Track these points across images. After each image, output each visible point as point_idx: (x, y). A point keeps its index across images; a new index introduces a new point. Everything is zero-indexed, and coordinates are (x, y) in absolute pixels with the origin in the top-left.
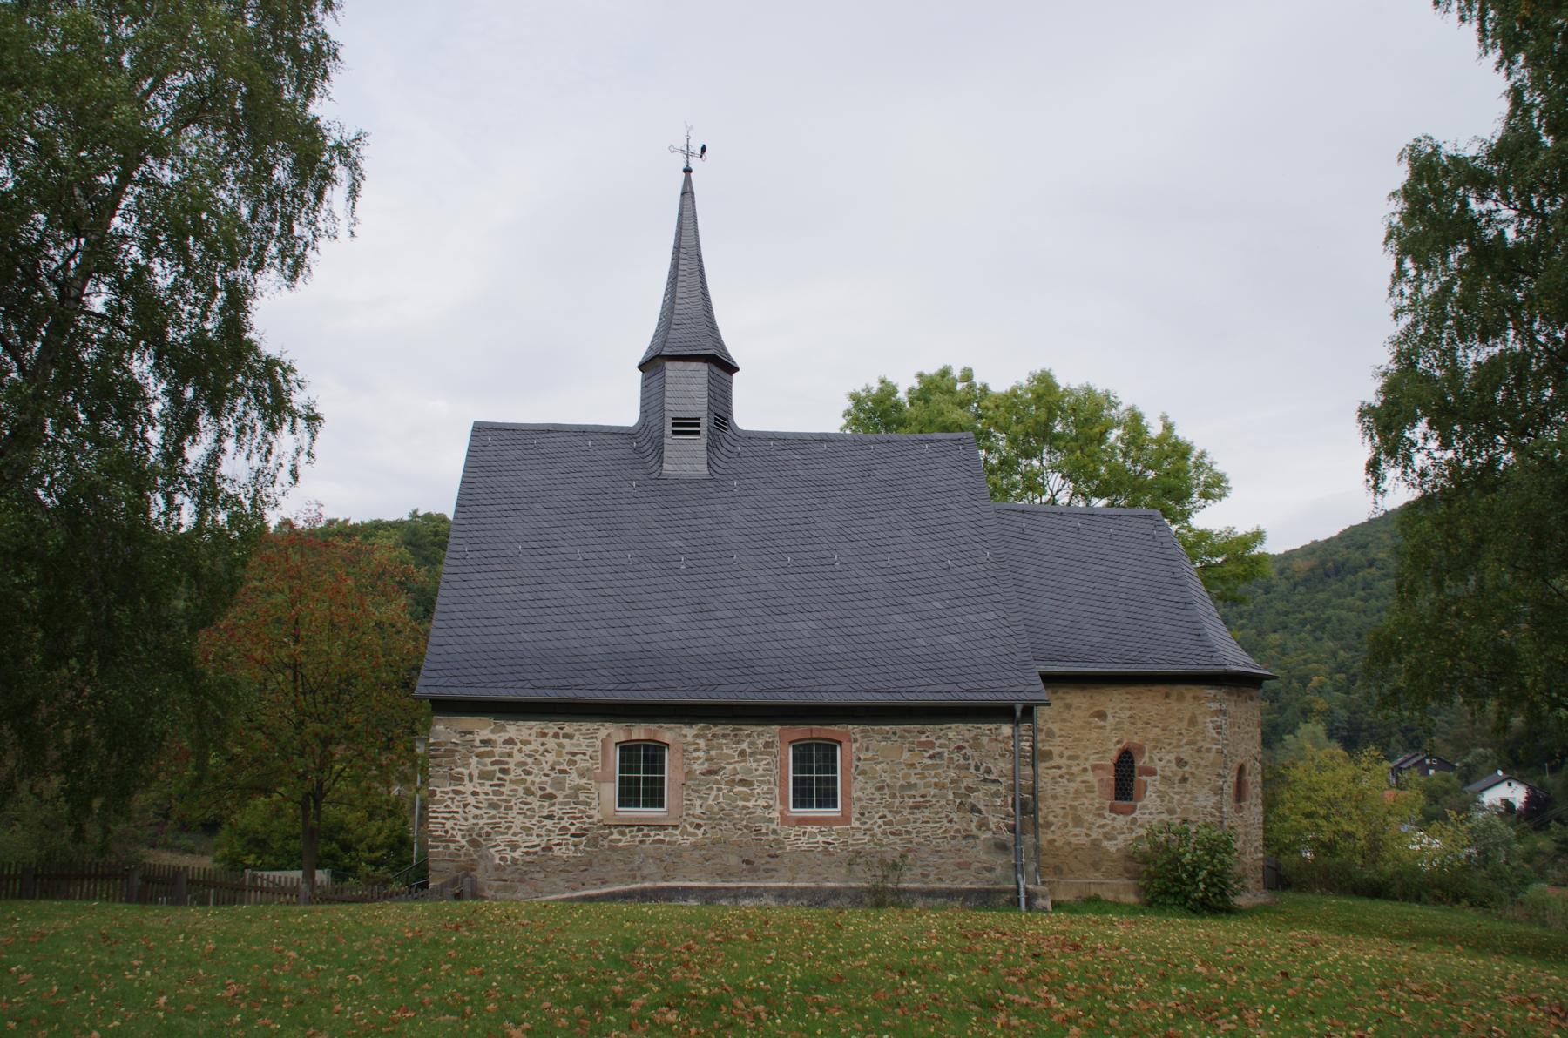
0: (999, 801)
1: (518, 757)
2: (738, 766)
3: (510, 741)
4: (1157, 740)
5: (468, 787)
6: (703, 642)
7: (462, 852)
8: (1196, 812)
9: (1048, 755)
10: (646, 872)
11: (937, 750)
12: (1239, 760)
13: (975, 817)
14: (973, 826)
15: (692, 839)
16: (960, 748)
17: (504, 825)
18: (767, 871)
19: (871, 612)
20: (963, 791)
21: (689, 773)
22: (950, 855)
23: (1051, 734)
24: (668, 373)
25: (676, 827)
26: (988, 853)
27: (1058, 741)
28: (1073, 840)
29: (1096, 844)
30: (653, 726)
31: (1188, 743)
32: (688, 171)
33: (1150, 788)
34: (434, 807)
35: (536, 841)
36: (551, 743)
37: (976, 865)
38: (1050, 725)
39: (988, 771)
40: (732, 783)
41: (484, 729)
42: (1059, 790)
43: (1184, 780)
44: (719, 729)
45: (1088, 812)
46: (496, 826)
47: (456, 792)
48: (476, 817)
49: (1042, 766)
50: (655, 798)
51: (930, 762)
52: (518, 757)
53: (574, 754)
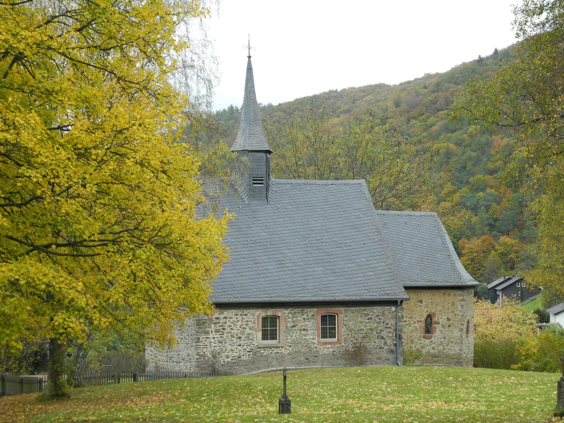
0: (391, 335)
1: (228, 324)
2: (303, 324)
4: (440, 311)
5: (211, 336)
8: (453, 338)
10: (273, 364)
11: (370, 316)
13: (383, 341)
15: (288, 351)
16: (378, 316)
17: (224, 349)
18: (313, 362)
20: (379, 331)
21: (287, 327)
25: (282, 347)
26: (387, 354)
27: (405, 311)
30: (275, 310)
31: (452, 312)
32: (249, 57)
33: (437, 329)
35: (236, 354)
36: (240, 318)
39: (387, 324)
40: (300, 330)
43: (449, 326)
44: (296, 310)
45: (416, 338)
48: (214, 347)
50: (274, 337)
52: (228, 324)
53: (248, 321)
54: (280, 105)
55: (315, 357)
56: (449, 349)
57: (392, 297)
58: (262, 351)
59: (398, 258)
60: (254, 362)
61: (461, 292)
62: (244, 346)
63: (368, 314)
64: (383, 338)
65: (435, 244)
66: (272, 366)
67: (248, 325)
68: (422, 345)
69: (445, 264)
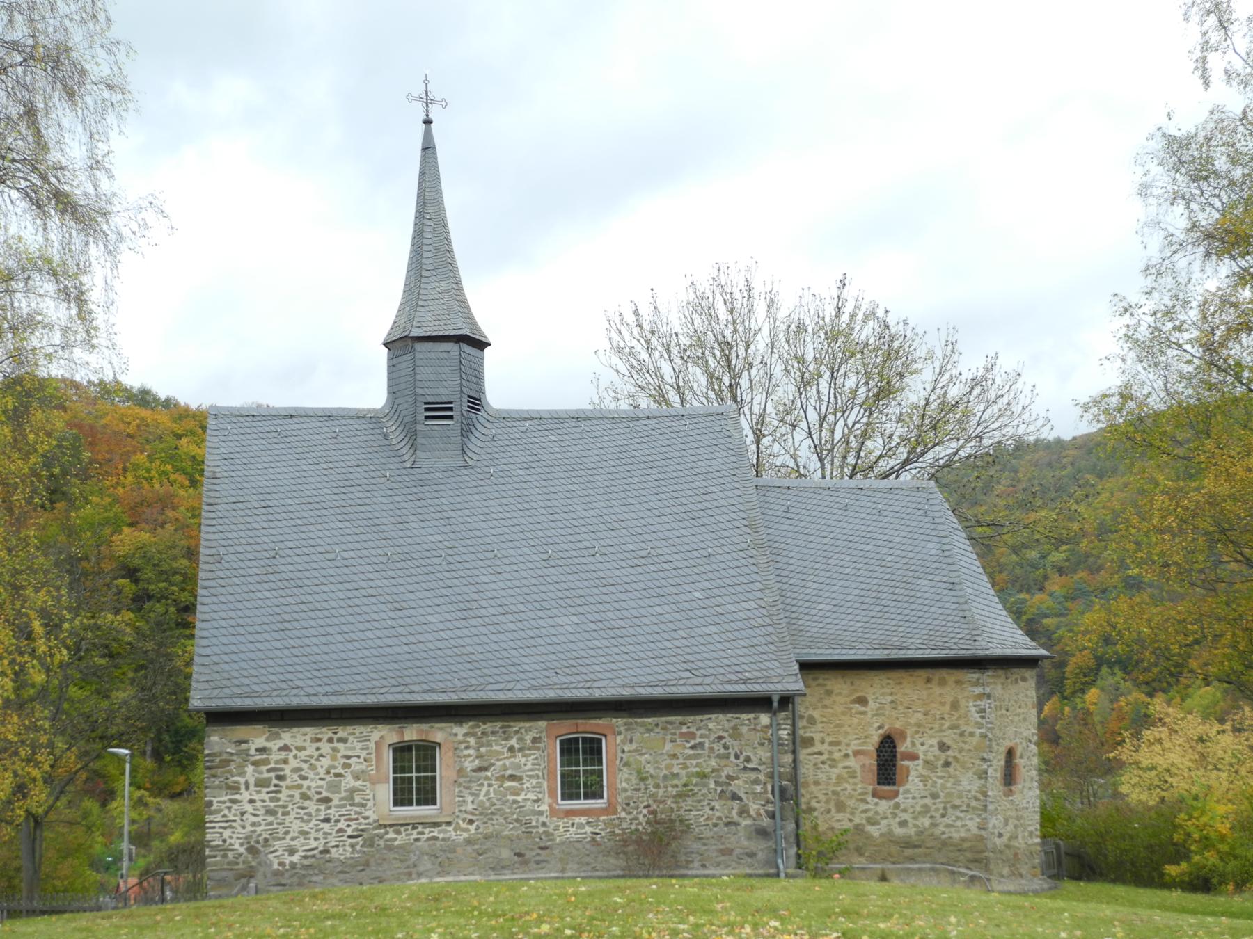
0: (758, 789)
1: (293, 763)
2: (507, 762)
3: (285, 748)
4: (919, 725)
5: (245, 796)
6: (468, 640)
7: (241, 860)
8: (960, 797)
9: (809, 742)
10: (421, 869)
11: (698, 740)
12: (1008, 744)
13: (736, 804)
14: (734, 813)
15: (465, 835)
16: (720, 738)
17: (281, 830)
18: (538, 863)
19: (632, 604)
20: (723, 779)
21: (461, 772)
22: (712, 841)
23: (812, 721)
24: (418, 355)
25: (449, 824)
26: (749, 838)
27: (819, 727)
28: (837, 825)
29: (859, 829)
30: (425, 727)
31: (952, 727)
32: (428, 122)
33: (913, 773)
34: (211, 818)
35: (314, 844)
36: (326, 748)
37: (737, 851)
38: (811, 712)
39: (748, 760)
40: (502, 778)
41: (257, 737)
42: (822, 776)
43: (947, 764)
44: (488, 727)
45: (851, 797)
46: (273, 832)
47: (234, 801)
48: (253, 824)
49: (803, 754)
50: (428, 797)
51: (691, 752)
52: (293, 763)
53: (349, 757)
54: (1074, 438)
55: (542, 848)
56: (948, 826)
57: (758, 687)
58: (391, 835)
59: (808, 591)
60: (367, 864)
61: (977, 676)
62: (337, 821)
63: (693, 736)
64: (734, 797)
65: (919, 556)
66: (420, 875)
67: (349, 766)
68: (870, 814)
69: (939, 604)
